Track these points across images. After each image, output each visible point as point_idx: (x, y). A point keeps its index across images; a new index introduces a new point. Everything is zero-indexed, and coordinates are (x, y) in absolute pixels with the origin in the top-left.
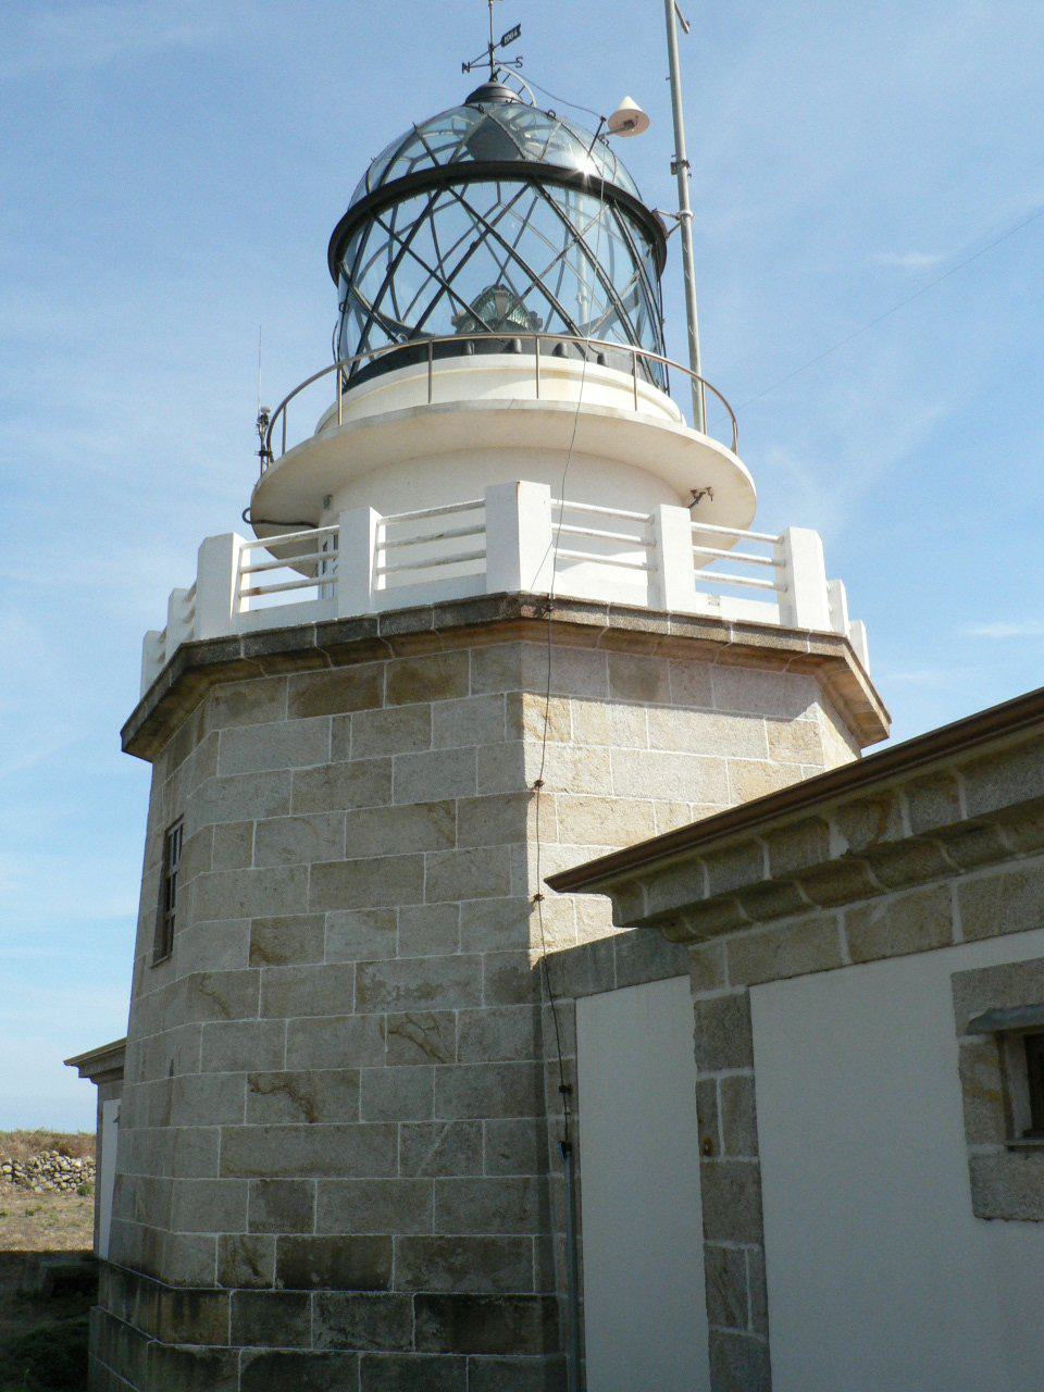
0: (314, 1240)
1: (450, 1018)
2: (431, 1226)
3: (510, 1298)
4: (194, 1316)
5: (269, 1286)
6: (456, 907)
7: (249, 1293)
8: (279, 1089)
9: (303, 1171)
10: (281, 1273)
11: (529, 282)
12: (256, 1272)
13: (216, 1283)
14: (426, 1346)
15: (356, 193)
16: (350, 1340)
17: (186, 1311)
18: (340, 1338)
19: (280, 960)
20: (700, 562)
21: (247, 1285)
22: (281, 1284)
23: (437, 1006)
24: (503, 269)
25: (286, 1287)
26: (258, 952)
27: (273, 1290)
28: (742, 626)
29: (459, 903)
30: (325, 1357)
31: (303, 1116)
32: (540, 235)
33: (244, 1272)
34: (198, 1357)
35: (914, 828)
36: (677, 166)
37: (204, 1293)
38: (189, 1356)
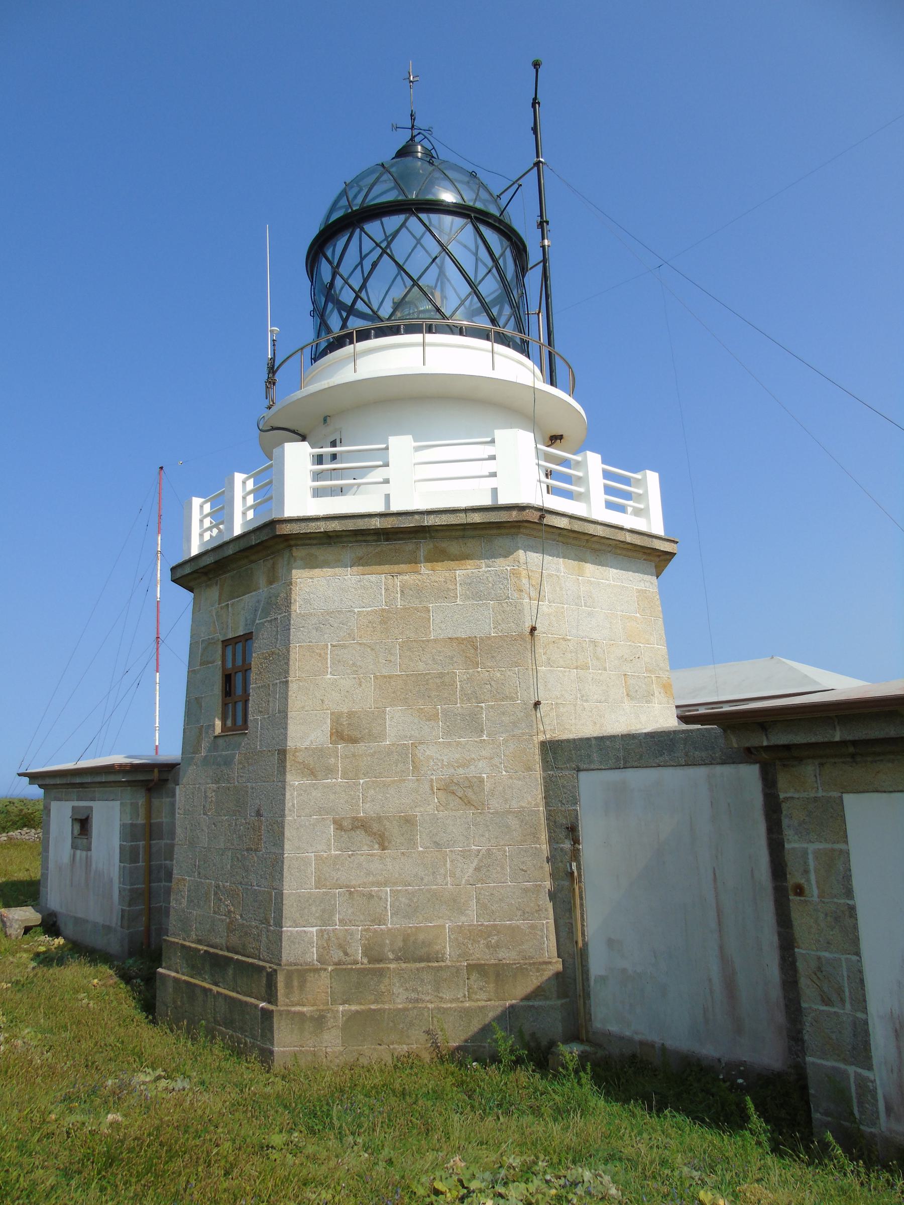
0: (389, 930)
1: (481, 781)
2: (471, 916)
3: (534, 963)
4: (302, 987)
5: (356, 962)
6: (482, 707)
7: (342, 970)
8: (357, 828)
9: (378, 884)
10: (365, 954)
11: (439, 249)
12: (346, 954)
13: (316, 962)
14: (474, 997)
15: (333, 208)
16: (421, 996)
17: (295, 983)
18: (413, 995)
19: (354, 741)
20: (608, 490)
21: (338, 963)
22: (365, 961)
23: (472, 771)
24: (418, 242)
25: (369, 962)
26: (339, 735)
27: (359, 966)
28: (632, 531)
29: (483, 705)
30: (405, 1009)
31: (377, 846)
32: (465, 246)
33: (337, 955)
34: (308, 1015)
35: (417, 196)
36: (535, 102)
37: (310, 970)
38: (302, 1014)
